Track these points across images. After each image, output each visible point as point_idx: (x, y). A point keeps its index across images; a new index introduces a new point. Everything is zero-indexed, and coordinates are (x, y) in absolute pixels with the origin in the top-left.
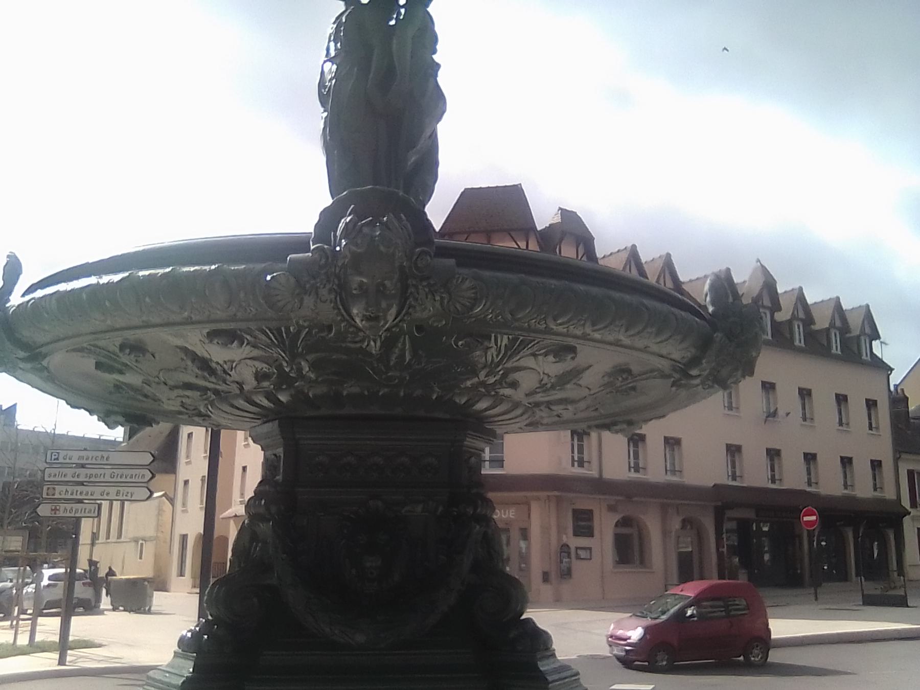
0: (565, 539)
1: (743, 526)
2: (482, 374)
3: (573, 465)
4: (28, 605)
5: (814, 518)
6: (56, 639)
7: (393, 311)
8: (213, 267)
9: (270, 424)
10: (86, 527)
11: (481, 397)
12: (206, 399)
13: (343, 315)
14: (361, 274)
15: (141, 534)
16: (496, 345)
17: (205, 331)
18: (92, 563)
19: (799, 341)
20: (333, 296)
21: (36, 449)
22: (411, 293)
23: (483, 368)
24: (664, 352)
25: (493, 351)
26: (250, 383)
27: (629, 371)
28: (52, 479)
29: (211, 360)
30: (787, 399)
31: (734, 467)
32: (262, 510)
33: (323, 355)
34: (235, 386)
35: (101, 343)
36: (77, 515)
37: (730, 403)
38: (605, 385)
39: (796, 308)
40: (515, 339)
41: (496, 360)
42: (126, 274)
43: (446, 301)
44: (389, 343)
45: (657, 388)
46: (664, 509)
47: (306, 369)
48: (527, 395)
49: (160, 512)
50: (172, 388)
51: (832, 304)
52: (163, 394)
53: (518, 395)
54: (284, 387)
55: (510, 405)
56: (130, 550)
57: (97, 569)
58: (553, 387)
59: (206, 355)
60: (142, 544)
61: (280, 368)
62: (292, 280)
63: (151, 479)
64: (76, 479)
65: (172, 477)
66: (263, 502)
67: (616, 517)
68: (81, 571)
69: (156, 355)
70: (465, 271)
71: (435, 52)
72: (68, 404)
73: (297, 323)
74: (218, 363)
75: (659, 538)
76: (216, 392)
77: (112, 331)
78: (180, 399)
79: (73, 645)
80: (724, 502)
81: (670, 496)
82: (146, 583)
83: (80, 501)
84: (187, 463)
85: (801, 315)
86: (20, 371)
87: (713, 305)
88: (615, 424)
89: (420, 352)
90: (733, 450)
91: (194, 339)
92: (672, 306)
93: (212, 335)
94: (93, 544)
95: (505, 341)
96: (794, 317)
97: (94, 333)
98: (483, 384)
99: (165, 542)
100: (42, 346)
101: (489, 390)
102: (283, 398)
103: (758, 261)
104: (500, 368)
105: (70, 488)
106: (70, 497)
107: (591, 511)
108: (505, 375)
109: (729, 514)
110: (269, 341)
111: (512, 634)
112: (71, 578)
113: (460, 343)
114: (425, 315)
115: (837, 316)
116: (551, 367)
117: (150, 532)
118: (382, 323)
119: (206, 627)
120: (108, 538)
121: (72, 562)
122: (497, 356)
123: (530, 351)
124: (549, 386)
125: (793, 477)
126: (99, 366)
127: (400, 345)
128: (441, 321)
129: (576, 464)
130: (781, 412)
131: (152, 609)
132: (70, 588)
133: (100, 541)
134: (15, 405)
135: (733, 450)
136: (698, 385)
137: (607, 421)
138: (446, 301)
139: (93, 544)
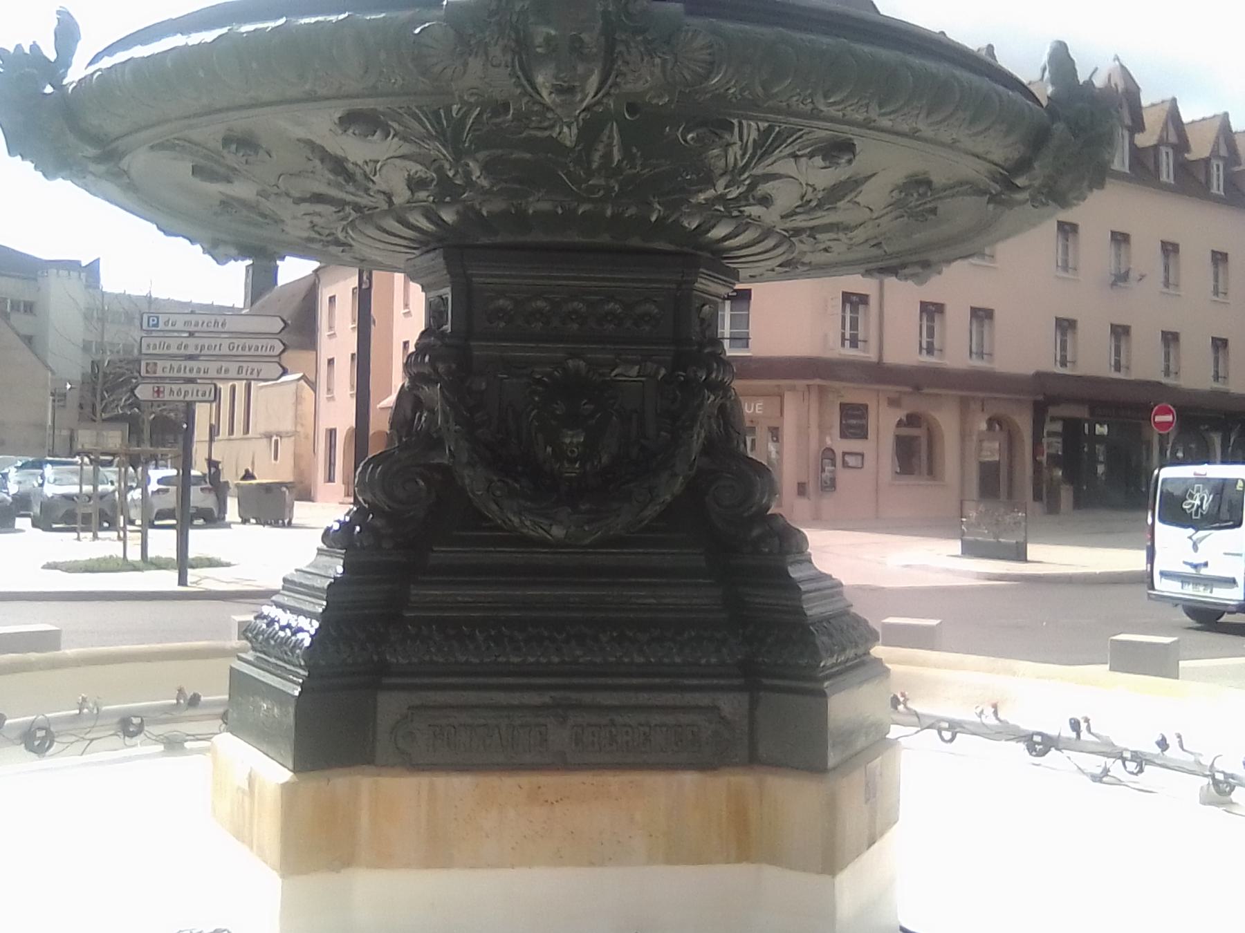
0: (828, 441)
1: (1072, 429)
2: (721, 183)
3: (843, 345)
4: (135, 514)
5: (1169, 418)
6: (173, 554)
7: (594, 81)
8: (342, 17)
9: (432, 255)
10: (203, 414)
11: (718, 219)
12: (342, 219)
13: (523, 87)
14: (548, 23)
15: (273, 428)
16: (741, 139)
17: (338, 115)
18: (212, 463)
19: (1167, 174)
20: (509, 58)
21: (129, 318)
22: (620, 52)
23: (722, 175)
24: (980, 149)
25: (735, 150)
26: (402, 195)
27: (928, 183)
28: (151, 351)
29: (346, 159)
30: (1145, 256)
31: (1064, 348)
32: (427, 370)
33: (500, 152)
34: (382, 197)
35: (195, 135)
36: (188, 398)
37: (1066, 262)
38: (894, 204)
39: (1165, 127)
40: (770, 129)
41: (741, 164)
42: (225, 30)
43: (669, 67)
44: (591, 131)
45: (962, 211)
46: (964, 404)
47: (476, 173)
48: (782, 217)
49: (298, 400)
50: (299, 201)
51: (1217, 123)
52: (286, 210)
53: (770, 216)
54: (448, 199)
55: (759, 231)
56: (262, 448)
57: (218, 472)
58: (819, 206)
59: (340, 153)
60: (276, 442)
61: (440, 170)
62: (451, 32)
63: (283, 351)
64: (182, 351)
65: (312, 355)
66: (427, 359)
67: (901, 414)
68: (199, 474)
69: (273, 154)
70: (696, 22)
72: (159, 228)
73: (461, 97)
74: (356, 164)
75: (959, 439)
76: (358, 208)
77: (210, 114)
78: (308, 218)
79: (194, 563)
80: (1046, 395)
81: (976, 387)
82: (284, 489)
83: (191, 381)
84: (330, 336)
85: (1173, 138)
86: (90, 178)
87: (1053, 84)
88: (904, 266)
89: (635, 150)
90: (1066, 326)
91: (320, 125)
92: (996, 81)
93: (349, 120)
94: (211, 440)
95: (754, 135)
96: (1162, 142)
97: (188, 117)
98: (721, 198)
99: (307, 437)
100: (117, 139)
101: (730, 208)
102: (448, 216)
103: (1117, 58)
104: (746, 175)
105: (176, 364)
106: (175, 374)
107: (866, 407)
108: (752, 187)
109: (1053, 411)
110: (424, 131)
111: (756, 532)
112: (185, 481)
113: (690, 136)
114: (640, 86)
115: (1221, 139)
116: (821, 176)
117: (287, 426)
118: (579, 97)
119: (359, 515)
120: (231, 431)
121: (186, 463)
122: (743, 155)
123: (788, 151)
124: (814, 204)
125: (1145, 364)
126: (196, 171)
127: (605, 139)
128: (660, 96)
130: (1134, 275)
131: (294, 521)
132: (184, 496)
133: (220, 437)
134: (98, 260)
135: (1066, 326)
136: (1026, 201)
137: (894, 262)
138: (669, 67)
139: (211, 440)
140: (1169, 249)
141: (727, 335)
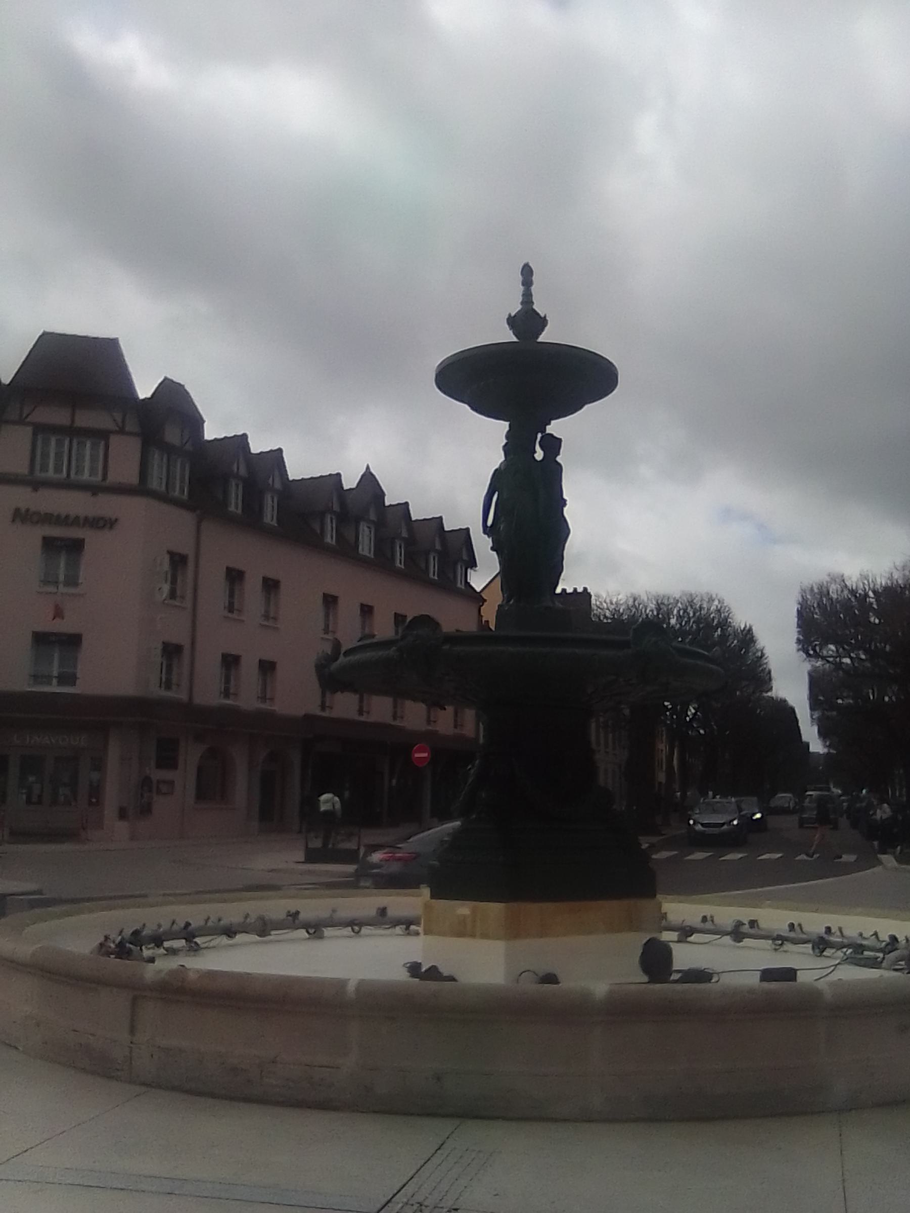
71: (558, 454)
103: (368, 468)
129: (163, 685)
140: (235, 577)
141: (55, 673)
